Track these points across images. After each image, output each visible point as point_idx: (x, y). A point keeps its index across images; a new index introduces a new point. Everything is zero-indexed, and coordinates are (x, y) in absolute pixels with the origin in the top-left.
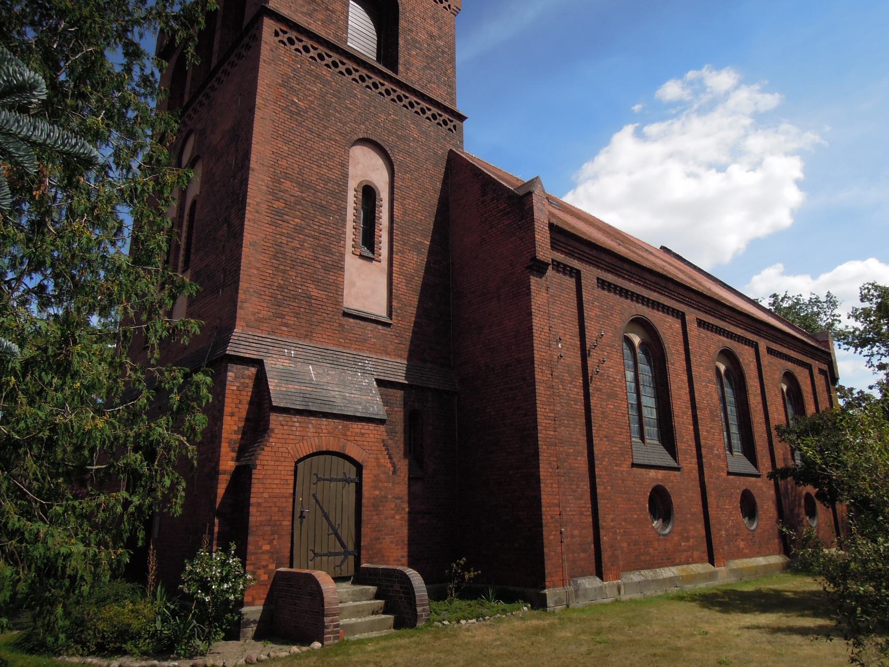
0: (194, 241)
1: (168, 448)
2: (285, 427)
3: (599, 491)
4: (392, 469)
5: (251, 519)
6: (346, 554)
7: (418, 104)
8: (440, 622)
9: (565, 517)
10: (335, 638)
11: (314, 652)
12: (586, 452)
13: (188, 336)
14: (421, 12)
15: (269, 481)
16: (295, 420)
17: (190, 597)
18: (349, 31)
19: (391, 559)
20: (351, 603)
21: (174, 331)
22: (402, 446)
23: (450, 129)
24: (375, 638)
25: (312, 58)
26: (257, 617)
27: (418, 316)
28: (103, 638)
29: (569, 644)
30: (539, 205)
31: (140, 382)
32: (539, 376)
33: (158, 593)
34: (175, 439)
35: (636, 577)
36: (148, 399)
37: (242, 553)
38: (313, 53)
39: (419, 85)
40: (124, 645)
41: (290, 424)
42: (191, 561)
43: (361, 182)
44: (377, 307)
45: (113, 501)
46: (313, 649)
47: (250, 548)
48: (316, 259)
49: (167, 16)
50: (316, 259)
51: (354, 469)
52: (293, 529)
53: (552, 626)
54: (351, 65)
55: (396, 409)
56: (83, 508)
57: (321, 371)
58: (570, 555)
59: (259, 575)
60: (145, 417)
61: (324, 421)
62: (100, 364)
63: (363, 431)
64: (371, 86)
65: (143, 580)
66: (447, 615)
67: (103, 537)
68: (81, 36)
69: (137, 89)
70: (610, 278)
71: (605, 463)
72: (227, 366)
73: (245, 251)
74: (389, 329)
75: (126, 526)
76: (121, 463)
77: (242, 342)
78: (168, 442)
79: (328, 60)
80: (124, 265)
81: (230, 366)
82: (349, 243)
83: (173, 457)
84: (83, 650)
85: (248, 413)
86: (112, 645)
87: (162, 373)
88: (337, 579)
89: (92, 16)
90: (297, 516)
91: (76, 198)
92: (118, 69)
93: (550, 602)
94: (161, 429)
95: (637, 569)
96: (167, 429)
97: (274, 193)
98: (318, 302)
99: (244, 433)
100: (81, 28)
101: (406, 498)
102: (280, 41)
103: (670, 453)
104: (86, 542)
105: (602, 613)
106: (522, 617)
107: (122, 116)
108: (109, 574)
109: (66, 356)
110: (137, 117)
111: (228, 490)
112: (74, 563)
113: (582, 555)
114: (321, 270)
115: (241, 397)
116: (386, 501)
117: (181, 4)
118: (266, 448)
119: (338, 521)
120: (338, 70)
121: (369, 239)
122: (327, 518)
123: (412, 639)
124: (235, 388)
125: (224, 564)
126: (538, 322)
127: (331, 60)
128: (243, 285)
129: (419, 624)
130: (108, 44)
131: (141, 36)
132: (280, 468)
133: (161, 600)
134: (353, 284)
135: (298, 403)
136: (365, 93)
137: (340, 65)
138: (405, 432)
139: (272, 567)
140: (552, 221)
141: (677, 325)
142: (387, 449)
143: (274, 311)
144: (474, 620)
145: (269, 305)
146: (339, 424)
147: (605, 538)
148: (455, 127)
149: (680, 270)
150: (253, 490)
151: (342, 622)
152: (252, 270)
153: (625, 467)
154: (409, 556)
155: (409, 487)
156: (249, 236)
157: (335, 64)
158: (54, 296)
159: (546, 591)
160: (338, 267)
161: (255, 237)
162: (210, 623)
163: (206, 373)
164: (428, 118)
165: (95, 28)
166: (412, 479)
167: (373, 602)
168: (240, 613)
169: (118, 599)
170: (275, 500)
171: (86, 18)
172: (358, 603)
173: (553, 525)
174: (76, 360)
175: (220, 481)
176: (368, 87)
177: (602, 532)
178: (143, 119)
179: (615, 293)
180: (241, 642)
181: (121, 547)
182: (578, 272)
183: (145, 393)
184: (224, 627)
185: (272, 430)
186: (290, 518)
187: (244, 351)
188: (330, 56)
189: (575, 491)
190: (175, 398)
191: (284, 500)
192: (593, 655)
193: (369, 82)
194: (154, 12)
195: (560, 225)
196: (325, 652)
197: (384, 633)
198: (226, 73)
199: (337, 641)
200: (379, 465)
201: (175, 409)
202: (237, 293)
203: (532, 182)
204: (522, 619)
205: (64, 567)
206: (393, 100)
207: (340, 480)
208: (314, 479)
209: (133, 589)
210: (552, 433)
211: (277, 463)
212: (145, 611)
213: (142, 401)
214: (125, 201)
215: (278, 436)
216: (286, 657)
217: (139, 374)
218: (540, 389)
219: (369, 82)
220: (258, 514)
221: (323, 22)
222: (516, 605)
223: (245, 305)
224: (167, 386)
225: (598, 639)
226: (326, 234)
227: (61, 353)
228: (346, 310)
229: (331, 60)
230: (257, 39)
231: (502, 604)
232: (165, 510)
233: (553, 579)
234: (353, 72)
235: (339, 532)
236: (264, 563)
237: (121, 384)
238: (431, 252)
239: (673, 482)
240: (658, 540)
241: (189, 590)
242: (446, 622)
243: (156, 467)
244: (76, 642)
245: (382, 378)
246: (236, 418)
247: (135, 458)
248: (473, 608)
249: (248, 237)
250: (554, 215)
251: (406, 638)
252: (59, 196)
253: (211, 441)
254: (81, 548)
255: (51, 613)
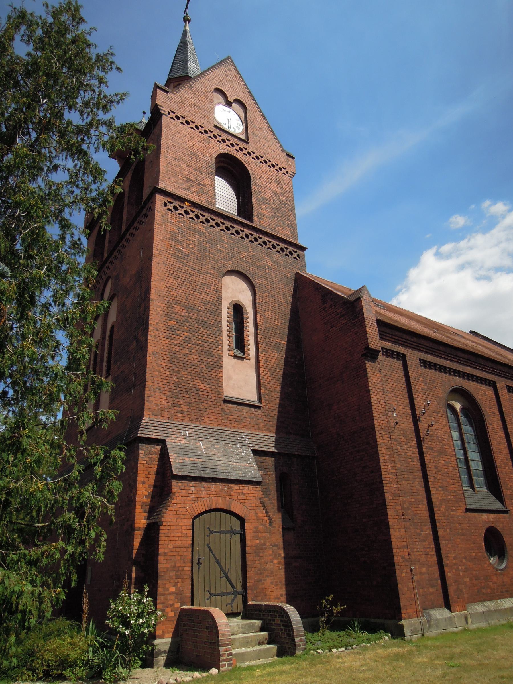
0: (113, 355)
1: (93, 508)
2: (184, 491)
3: (440, 533)
4: (268, 521)
5: (160, 566)
6: (236, 593)
7: (252, 235)
8: (315, 650)
9: (413, 557)
10: (230, 665)
11: (212, 677)
12: (425, 500)
13: (107, 422)
14: (267, 178)
15: (173, 535)
16: (191, 485)
17: (113, 632)
18: (216, 197)
19: (272, 597)
20: (241, 635)
21: (98, 421)
22: (275, 502)
23: (295, 258)
24: (262, 665)
25: (191, 218)
26: (167, 648)
27: (281, 399)
28: (48, 666)
29: (426, 668)
30: (367, 306)
31: (72, 457)
32: (381, 439)
33: (90, 629)
34: (99, 500)
35: (480, 608)
36: (79, 472)
37: (153, 594)
38: (191, 215)
39: (269, 228)
40: (64, 672)
41: (187, 488)
42: (115, 600)
43: (232, 302)
44: (250, 394)
45: (53, 550)
46: (211, 674)
47: (160, 590)
48: (201, 361)
49: (87, 200)
50: (201, 361)
51: (238, 522)
52: (192, 573)
53: (410, 652)
54: (219, 220)
55: (269, 473)
56: (31, 556)
57: (209, 446)
58: (421, 590)
59: (167, 613)
60: (77, 486)
61: (213, 485)
62: (44, 445)
63: (244, 491)
64: (234, 233)
65: (80, 619)
66: (320, 644)
67: (46, 580)
68: (29, 218)
69: (69, 250)
70: (430, 358)
71: (442, 510)
72: (139, 446)
73: (149, 358)
74: (259, 411)
75: (62, 570)
76: (59, 521)
77: (149, 427)
78: (93, 503)
79: (202, 219)
80: (60, 372)
81: (141, 446)
82: (225, 347)
83: (97, 515)
84: (33, 676)
85: (155, 481)
86: (55, 672)
87: (88, 451)
88: (230, 615)
89: (37, 203)
90: (195, 563)
91: (26, 327)
92: (56, 238)
93: (407, 632)
94: (88, 493)
95: (480, 601)
96: (93, 494)
97: (169, 315)
98: (204, 393)
99: (153, 497)
100: (29, 213)
101: (282, 545)
102: (168, 209)
103: (499, 501)
104: (33, 583)
105: (453, 641)
106: (383, 645)
107: (58, 269)
108: (50, 610)
109: (17, 438)
110: (68, 268)
111: (142, 543)
112: (24, 600)
113: (431, 590)
114: (205, 369)
115: (150, 469)
116: (265, 548)
117: (97, 190)
118: (169, 508)
119: (228, 566)
120: (210, 224)
121: (240, 343)
122: (219, 563)
123: (293, 666)
124: (145, 462)
125: (139, 602)
126: (375, 397)
127: (204, 218)
128: (148, 384)
129: (298, 653)
130: (49, 222)
131: (71, 214)
132: (181, 524)
133: (93, 634)
134: (230, 378)
135: (192, 471)
136: (230, 238)
137: (211, 221)
138: (277, 491)
139: (177, 605)
140: (378, 318)
141: (490, 392)
142: (264, 506)
143: (172, 402)
144: (343, 649)
145: (168, 398)
146: (225, 487)
147: (449, 575)
148: (298, 255)
149: (488, 348)
150: (160, 542)
151: (234, 651)
152: (155, 373)
153: (460, 512)
154: (287, 594)
155: (283, 536)
156: (152, 348)
157: (208, 221)
158: (13, 399)
159: (403, 622)
160: (218, 366)
161: (156, 348)
162: (130, 653)
163: (120, 449)
164: (278, 251)
165: (39, 212)
166: (285, 530)
167: (259, 634)
168: (153, 644)
169: (60, 634)
170: (178, 550)
171: (33, 205)
172: (247, 635)
173: (403, 564)
174: (24, 440)
175: (135, 536)
176: (232, 234)
177: (446, 569)
178: (74, 270)
179: (436, 370)
180: (155, 669)
181: (60, 588)
182: (404, 356)
183: (76, 466)
184: (141, 656)
185: (174, 494)
186: (190, 565)
187: (151, 433)
188: (203, 216)
189: (420, 534)
190: (98, 469)
191: (185, 550)
192: (447, 678)
193: (233, 231)
194: (79, 197)
195: (385, 320)
196: (221, 677)
197: (269, 660)
198: (132, 235)
199: (230, 668)
200: (258, 519)
201: (98, 478)
202: (145, 390)
203: (360, 290)
204: (384, 647)
205: (17, 604)
206: (251, 241)
207: (227, 532)
208: (208, 532)
209: (71, 625)
210: (395, 486)
211: (179, 520)
212: (77, 643)
213: (75, 473)
214: (61, 327)
215: (178, 498)
216: (190, 681)
217: (72, 452)
218: (382, 450)
219: (233, 231)
220: (166, 561)
221: (197, 193)
222: (378, 635)
223: (151, 399)
224: (92, 461)
225: (451, 663)
226: (208, 342)
227: (15, 436)
228: (226, 398)
229: (204, 218)
230: (152, 209)
231: (367, 635)
232: (92, 557)
233: (409, 611)
234: (221, 224)
235: (229, 575)
236: (171, 602)
237: (59, 460)
238: (289, 349)
239: (503, 523)
240: (496, 574)
241: (113, 624)
242: (320, 651)
243: (85, 523)
244: (28, 670)
245: (256, 449)
246: (146, 486)
247: (70, 516)
248: (341, 639)
249: (151, 348)
250: (380, 314)
251: (287, 665)
252: (15, 326)
253: (127, 502)
254: (30, 588)
255: (6, 641)
